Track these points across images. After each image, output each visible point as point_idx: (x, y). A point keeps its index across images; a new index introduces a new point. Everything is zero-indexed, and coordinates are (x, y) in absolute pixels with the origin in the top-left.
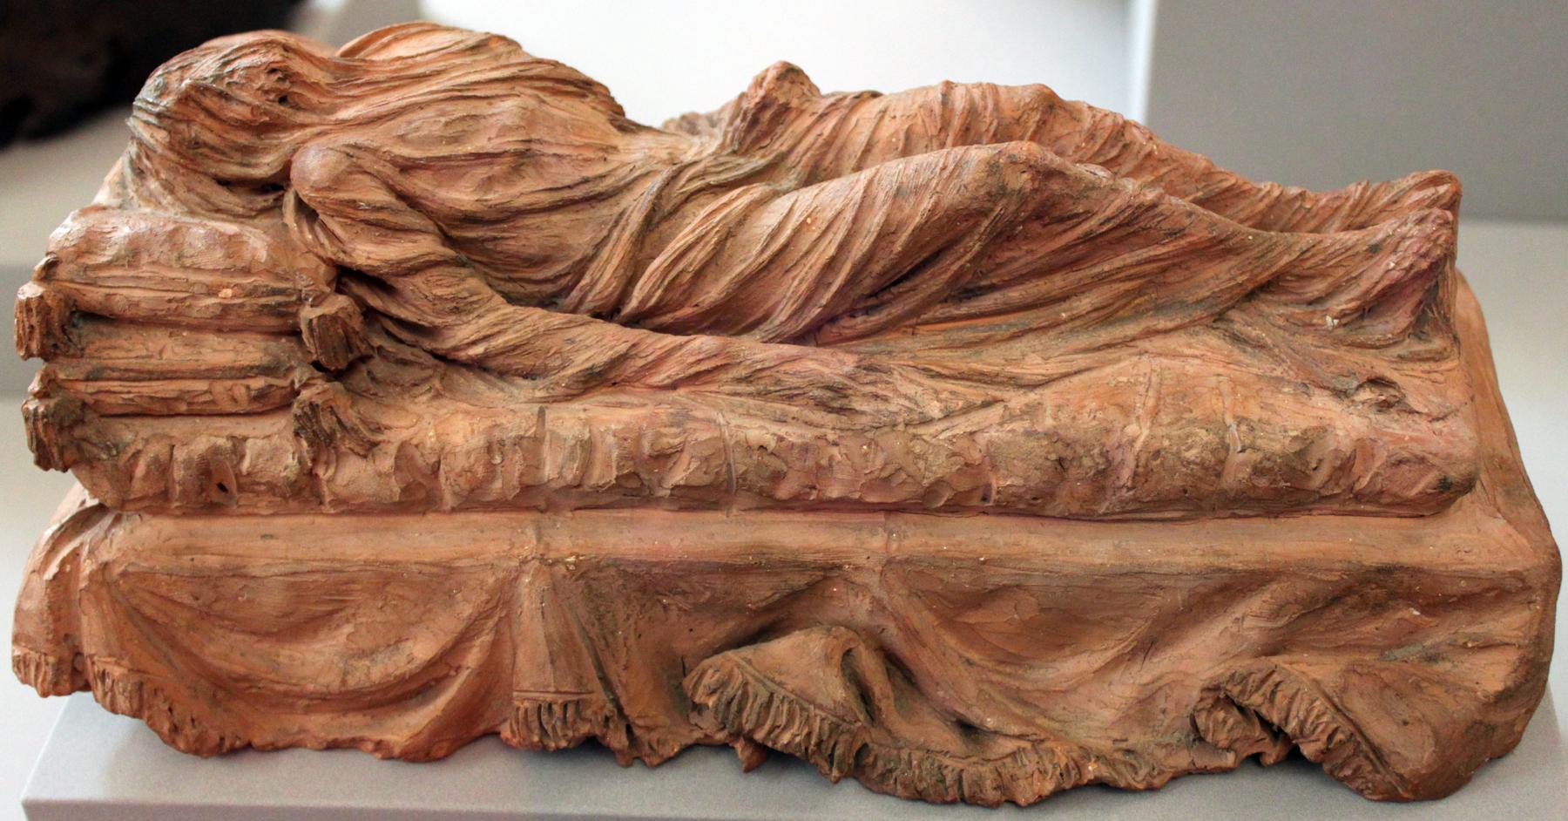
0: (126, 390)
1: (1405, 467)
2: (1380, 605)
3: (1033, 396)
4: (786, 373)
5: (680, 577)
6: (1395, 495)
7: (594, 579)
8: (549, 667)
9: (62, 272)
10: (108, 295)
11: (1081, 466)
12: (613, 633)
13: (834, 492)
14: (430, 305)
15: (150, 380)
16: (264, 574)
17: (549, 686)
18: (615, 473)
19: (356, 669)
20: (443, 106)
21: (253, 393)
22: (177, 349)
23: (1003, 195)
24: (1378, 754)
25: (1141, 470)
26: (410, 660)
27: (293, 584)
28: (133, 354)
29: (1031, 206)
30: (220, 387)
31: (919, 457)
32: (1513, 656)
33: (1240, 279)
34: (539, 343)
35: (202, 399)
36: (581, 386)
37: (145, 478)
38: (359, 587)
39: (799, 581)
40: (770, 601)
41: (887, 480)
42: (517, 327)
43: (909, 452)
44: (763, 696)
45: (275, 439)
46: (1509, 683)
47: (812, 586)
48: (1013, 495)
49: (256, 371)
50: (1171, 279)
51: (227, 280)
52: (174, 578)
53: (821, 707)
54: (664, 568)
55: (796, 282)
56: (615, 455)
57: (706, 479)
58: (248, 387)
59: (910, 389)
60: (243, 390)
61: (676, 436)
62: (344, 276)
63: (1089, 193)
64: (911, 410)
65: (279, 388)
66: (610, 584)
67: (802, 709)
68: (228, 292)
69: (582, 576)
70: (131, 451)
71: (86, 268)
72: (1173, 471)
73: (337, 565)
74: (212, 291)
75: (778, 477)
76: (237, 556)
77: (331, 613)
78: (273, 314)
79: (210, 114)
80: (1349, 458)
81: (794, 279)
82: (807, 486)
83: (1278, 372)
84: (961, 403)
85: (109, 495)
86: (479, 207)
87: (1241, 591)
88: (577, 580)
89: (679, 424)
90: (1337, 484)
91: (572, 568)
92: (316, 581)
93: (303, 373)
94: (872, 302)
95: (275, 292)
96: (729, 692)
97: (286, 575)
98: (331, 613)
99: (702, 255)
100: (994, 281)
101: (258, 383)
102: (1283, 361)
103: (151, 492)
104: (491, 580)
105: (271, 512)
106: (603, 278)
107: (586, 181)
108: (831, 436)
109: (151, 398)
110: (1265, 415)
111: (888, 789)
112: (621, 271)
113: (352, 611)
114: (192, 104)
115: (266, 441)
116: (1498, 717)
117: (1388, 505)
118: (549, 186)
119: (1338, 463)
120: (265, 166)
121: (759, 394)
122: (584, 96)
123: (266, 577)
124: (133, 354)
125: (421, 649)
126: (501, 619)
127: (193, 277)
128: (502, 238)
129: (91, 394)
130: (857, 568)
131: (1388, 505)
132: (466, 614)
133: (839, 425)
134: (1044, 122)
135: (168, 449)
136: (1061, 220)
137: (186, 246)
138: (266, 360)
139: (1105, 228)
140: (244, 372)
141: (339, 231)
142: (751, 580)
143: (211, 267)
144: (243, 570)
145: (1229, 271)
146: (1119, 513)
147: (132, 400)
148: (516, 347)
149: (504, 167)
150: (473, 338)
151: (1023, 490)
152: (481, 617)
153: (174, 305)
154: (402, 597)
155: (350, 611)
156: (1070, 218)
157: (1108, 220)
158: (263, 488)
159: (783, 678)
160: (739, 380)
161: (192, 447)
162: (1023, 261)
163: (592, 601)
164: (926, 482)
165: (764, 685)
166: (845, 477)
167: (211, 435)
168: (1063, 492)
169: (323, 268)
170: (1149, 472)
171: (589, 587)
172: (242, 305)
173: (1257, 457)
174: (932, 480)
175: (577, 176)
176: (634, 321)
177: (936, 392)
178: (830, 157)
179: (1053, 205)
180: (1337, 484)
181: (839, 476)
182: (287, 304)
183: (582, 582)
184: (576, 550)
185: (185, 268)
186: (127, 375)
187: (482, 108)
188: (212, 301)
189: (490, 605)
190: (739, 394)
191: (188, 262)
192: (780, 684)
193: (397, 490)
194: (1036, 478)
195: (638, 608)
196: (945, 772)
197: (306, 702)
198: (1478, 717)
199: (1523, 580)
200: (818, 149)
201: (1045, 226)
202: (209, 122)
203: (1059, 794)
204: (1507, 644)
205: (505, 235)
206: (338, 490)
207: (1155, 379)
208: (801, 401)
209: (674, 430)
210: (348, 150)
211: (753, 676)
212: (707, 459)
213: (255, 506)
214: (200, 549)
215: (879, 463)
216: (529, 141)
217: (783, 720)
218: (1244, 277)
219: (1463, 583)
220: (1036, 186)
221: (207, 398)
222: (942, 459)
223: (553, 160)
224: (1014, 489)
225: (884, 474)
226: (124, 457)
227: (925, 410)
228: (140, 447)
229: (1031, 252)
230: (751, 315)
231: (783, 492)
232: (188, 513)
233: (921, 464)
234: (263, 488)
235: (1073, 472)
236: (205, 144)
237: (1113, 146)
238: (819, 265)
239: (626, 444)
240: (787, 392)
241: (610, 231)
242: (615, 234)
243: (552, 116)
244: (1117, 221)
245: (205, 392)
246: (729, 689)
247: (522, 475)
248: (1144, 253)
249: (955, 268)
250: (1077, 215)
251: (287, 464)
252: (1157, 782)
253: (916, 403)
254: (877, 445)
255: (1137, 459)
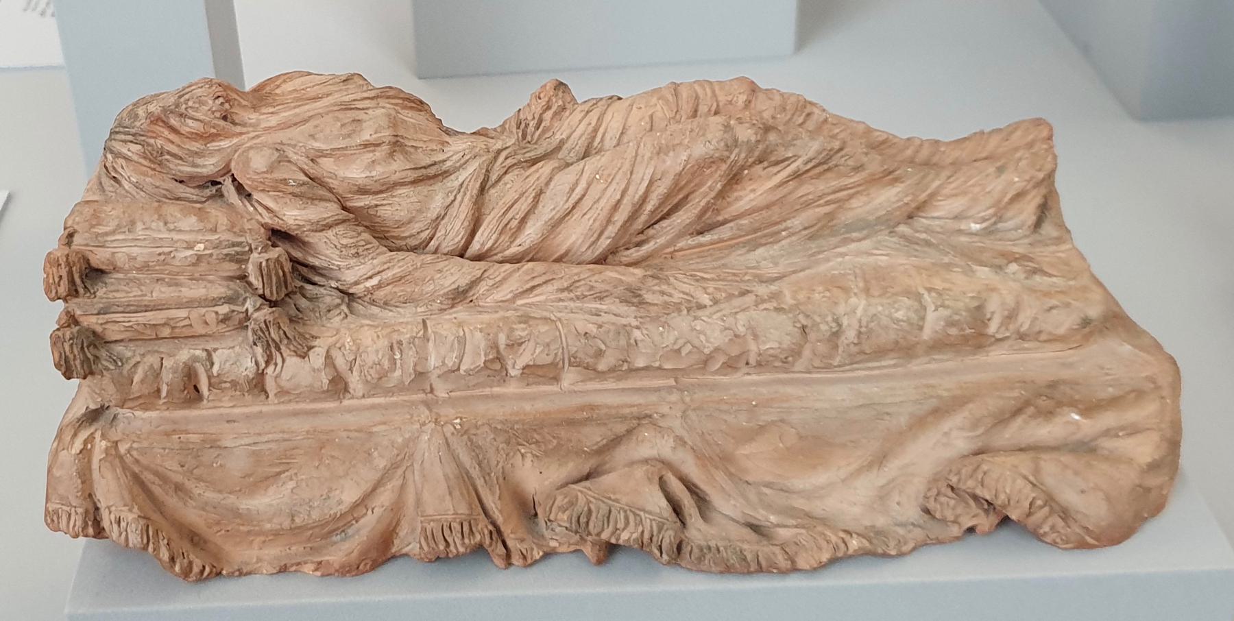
0: (126, 319)
1: (1054, 311)
2: (1051, 413)
3: (773, 288)
4: (596, 282)
5: (535, 430)
6: (1050, 333)
7: (475, 435)
8: (448, 497)
9: (77, 239)
10: (113, 253)
11: (819, 330)
12: (489, 474)
13: (640, 363)
14: (338, 252)
15: (146, 311)
16: (234, 445)
17: (449, 510)
18: (483, 359)
19: (300, 513)
20: (337, 114)
21: (221, 317)
22: (163, 289)
23: (736, 146)
24: (1066, 514)
25: (863, 330)
26: (340, 502)
27: (254, 452)
28: (131, 295)
29: (757, 154)
30: (195, 314)
31: (700, 332)
32: (1155, 437)
33: (906, 200)
34: (417, 274)
35: (182, 324)
36: (450, 302)
37: (142, 381)
38: (302, 452)
39: (621, 428)
40: (601, 444)
41: (678, 351)
42: (401, 264)
43: (693, 329)
44: (604, 509)
45: (237, 348)
46: (1156, 457)
47: (629, 432)
48: (771, 356)
49: (223, 300)
50: (854, 206)
51: (200, 237)
52: (167, 451)
53: (650, 513)
54: (523, 425)
55: (591, 221)
56: (482, 345)
57: (548, 360)
58: (217, 313)
59: (686, 288)
60: (214, 315)
61: (524, 330)
62: (278, 235)
63: (795, 142)
64: (689, 301)
65: (239, 313)
66: (485, 439)
67: (635, 514)
68: (201, 246)
69: (466, 432)
70: (133, 362)
71: (97, 235)
72: (886, 328)
73: (286, 436)
74: (190, 247)
75: (599, 354)
76: (212, 434)
77: (279, 474)
78: (231, 261)
79: (173, 130)
80: (1014, 309)
81: (589, 220)
82: (621, 360)
83: (946, 260)
84: (724, 295)
85: (114, 396)
86: (368, 182)
87: (947, 412)
88: (462, 435)
89: (525, 322)
90: (1007, 329)
91: (458, 427)
92: (270, 449)
93: (255, 302)
94: (642, 237)
95: (234, 245)
96: (578, 509)
97: (249, 445)
98: (279, 474)
99: (525, 205)
100: (726, 216)
101: (224, 309)
102: (949, 253)
103: (146, 392)
104: (400, 440)
105: (231, 404)
106: (452, 232)
107: (435, 164)
108: (634, 323)
109: (145, 324)
110: (947, 286)
111: (704, 568)
112: (466, 224)
113: (296, 471)
114: (161, 124)
115: (231, 350)
116: (1153, 481)
117: (1045, 341)
118: (413, 167)
119: (1006, 313)
120: (209, 166)
121: (578, 298)
122: (421, 111)
123: (235, 447)
124: (131, 295)
125: (349, 495)
126: (407, 467)
127: (176, 236)
128: (382, 205)
129: (101, 324)
130: (663, 416)
131: (1045, 341)
132: (381, 466)
133: (639, 314)
134: (750, 102)
135: (159, 360)
136: (777, 163)
137: (169, 216)
138: (230, 293)
139: (809, 166)
140: (215, 302)
141: (271, 204)
142: (587, 430)
143: (188, 229)
144: (218, 443)
145: (896, 195)
146: (848, 365)
147: (131, 327)
148: (401, 278)
149: (383, 153)
150: (370, 274)
151: (779, 350)
152: (394, 466)
153: (162, 257)
154: (332, 457)
155: (292, 472)
156: (782, 161)
157: (810, 160)
158: (228, 385)
159: (618, 496)
160: (562, 290)
161: (177, 357)
162: (747, 199)
163: (474, 451)
164: (707, 351)
165: (603, 502)
166: (649, 351)
167: (190, 349)
168: (807, 352)
169: (262, 230)
170: (870, 331)
171: (470, 440)
172: (211, 255)
173: (947, 313)
174: (712, 349)
175: (428, 161)
176: (479, 258)
177: (704, 288)
178: (598, 140)
179: (772, 152)
180: (1007, 329)
181: (644, 351)
182: (243, 253)
183: (465, 437)
184: (460, 415)
185: (170, 231)
186: (128, 310)
187: (360, 115)
188: (190, 252)
189: (399, 458)
190: (562, 300)
191: (172, 226)
192: (617, 501)
193: (326, 381)
194: (787, 342)
195: (504, 456)
196: (745, 553)
197: (262, 538)
198: (1137, 482)
199: (1154, 382)
200: (588, 134)
201: (765, 169)
202: (172, 137)
203: (833, 561)
204: (1148, 429)
205: (384, 202)
206: (283, 383)
207: (858, 271)
208: (607, 301)
209: (523, 326)
210: (277, 146)
211: (594, 497)
212: (548, 345)
213: (220, 400)
214: (183, 431)
215: (672, 339)
216: (397, 136)
217: (621, 525)
218: (909, 198)
219: (1111, 389)
220: (759, 138)
221: (186, 322)
222: (717, 333)
223: (412, 150)
224: (772, 352)
225: (676, 347)
226: (127, 367)
227: (699, 301)
228: (139, 359)
229: (753, 191)
230: (556, 252)
231: (602, 366)
232: (170, 405)
233: (702, 338)
234: (228, 385)
235: (812, 336)
236: (169, 153)
237: (799, 116)
238: (608, 207)
239: (490, 337)
240: (598, 295)
241: (455, 197)
242: (459, 198)
243: (406, 121)
244: (817, 161)
245: (185, 318)
246: (578, 507)
247: (415, 365)
248: (835, 184)
249: (702, 204)
250: (787, 159)
251: (247, 367)
252: (905, 549)
253: (692, 296)
254: (669, 326)
255: (860, 321)
